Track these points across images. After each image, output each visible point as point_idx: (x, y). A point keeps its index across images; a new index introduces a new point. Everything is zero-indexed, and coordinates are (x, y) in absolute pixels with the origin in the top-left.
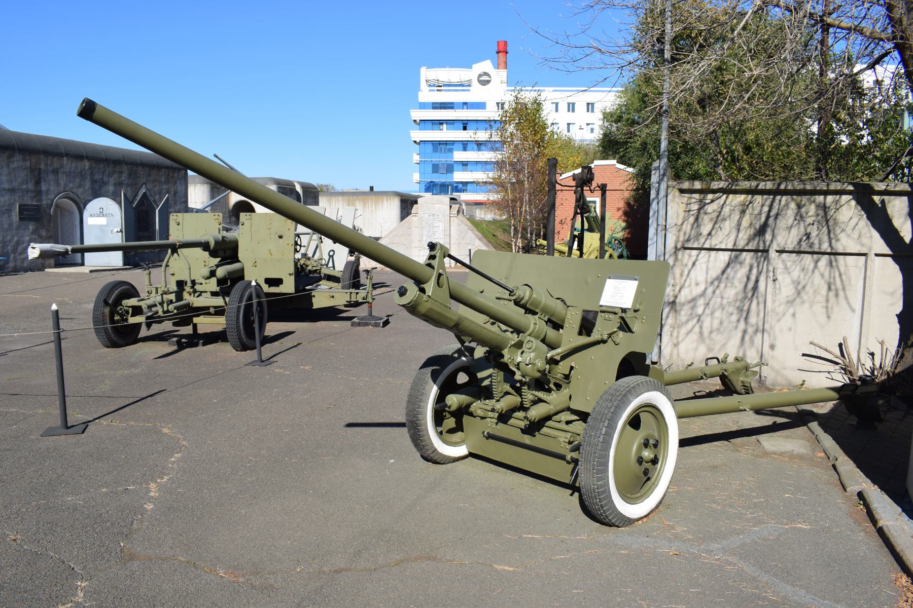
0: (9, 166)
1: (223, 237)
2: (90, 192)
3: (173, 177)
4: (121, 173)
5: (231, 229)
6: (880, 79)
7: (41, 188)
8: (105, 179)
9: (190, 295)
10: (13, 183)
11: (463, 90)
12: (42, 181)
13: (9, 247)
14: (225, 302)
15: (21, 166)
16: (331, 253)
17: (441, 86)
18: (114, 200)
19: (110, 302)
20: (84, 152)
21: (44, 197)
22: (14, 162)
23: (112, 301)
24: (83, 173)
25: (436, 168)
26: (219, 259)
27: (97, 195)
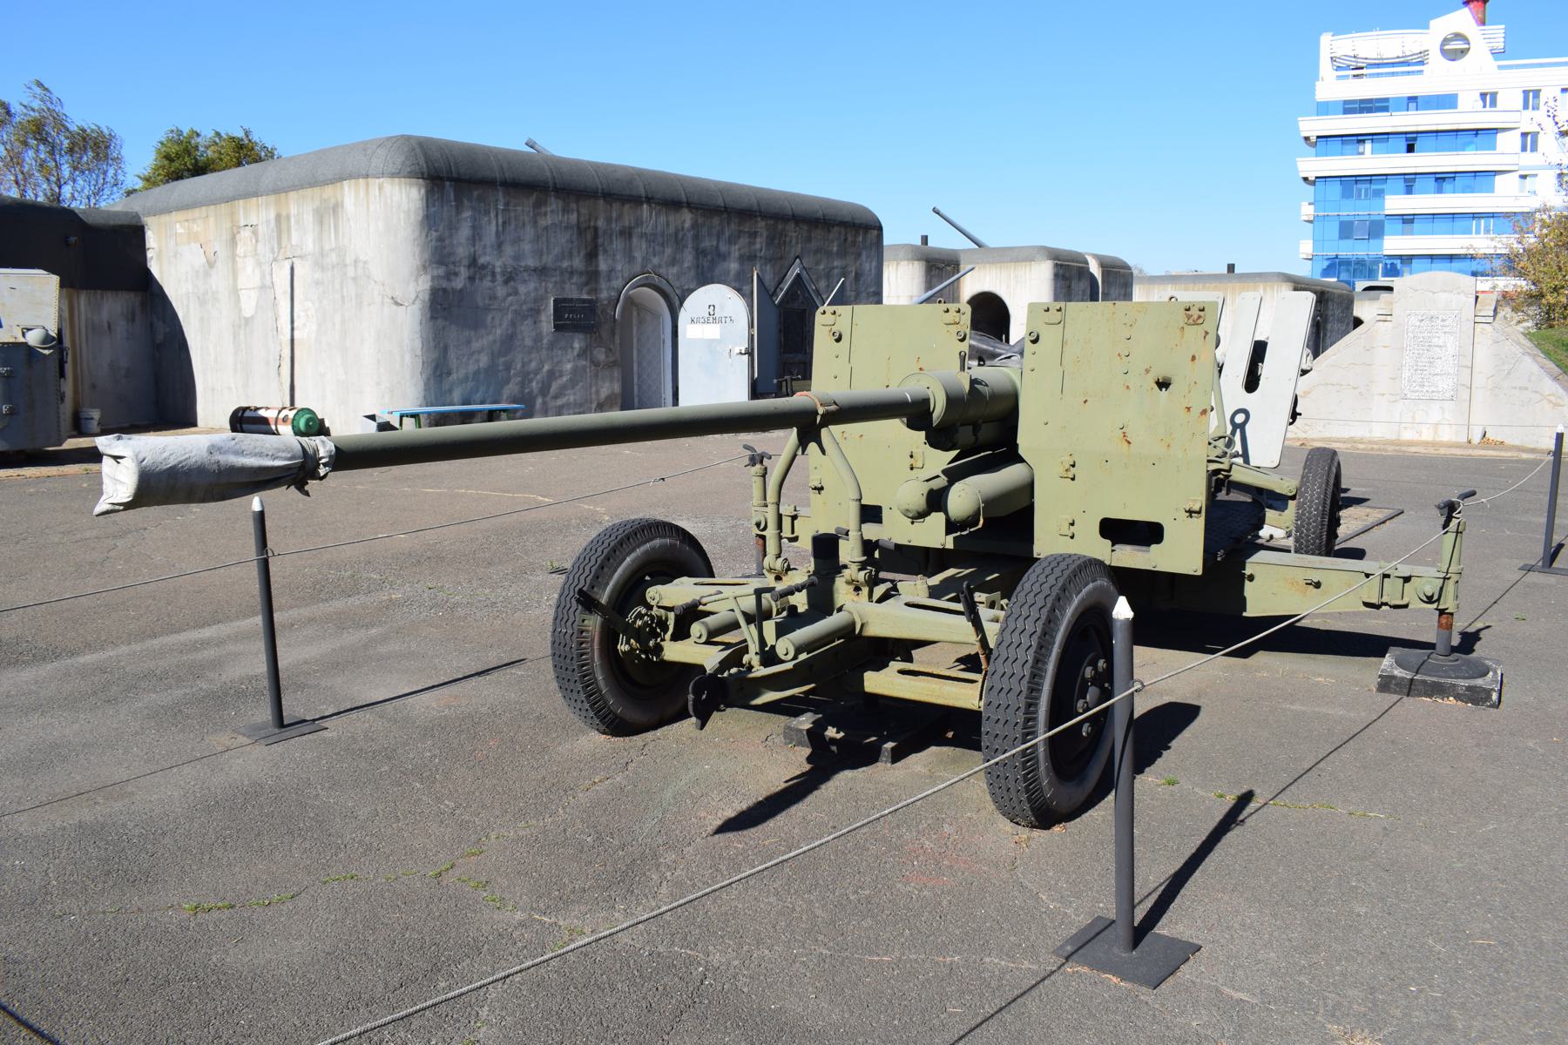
0: (536, 222)
1: (973, 382)
2: (693, 273)
3: (854, 243)
4: (754, 235)
5: (994, 356)
6: (312, 485)
7: (597, 266)
8: (723, 248)
9: (857, 589)
10: (544, 257)
11: (1409, 73)
12: (601, 253)
13: (534, 384)
14: (984, 642)
15: (561, 222)
16: (1240, 418)
17: (1362, 68)
18: (739, 290)
19: (604, 600)
20: (683, 196)
21: (603, 285)
22: (545, 214)
23: (610, 597)
24: (680, 236)
25: (1346, 230)
26: (954, 453)
27: (704, 279)
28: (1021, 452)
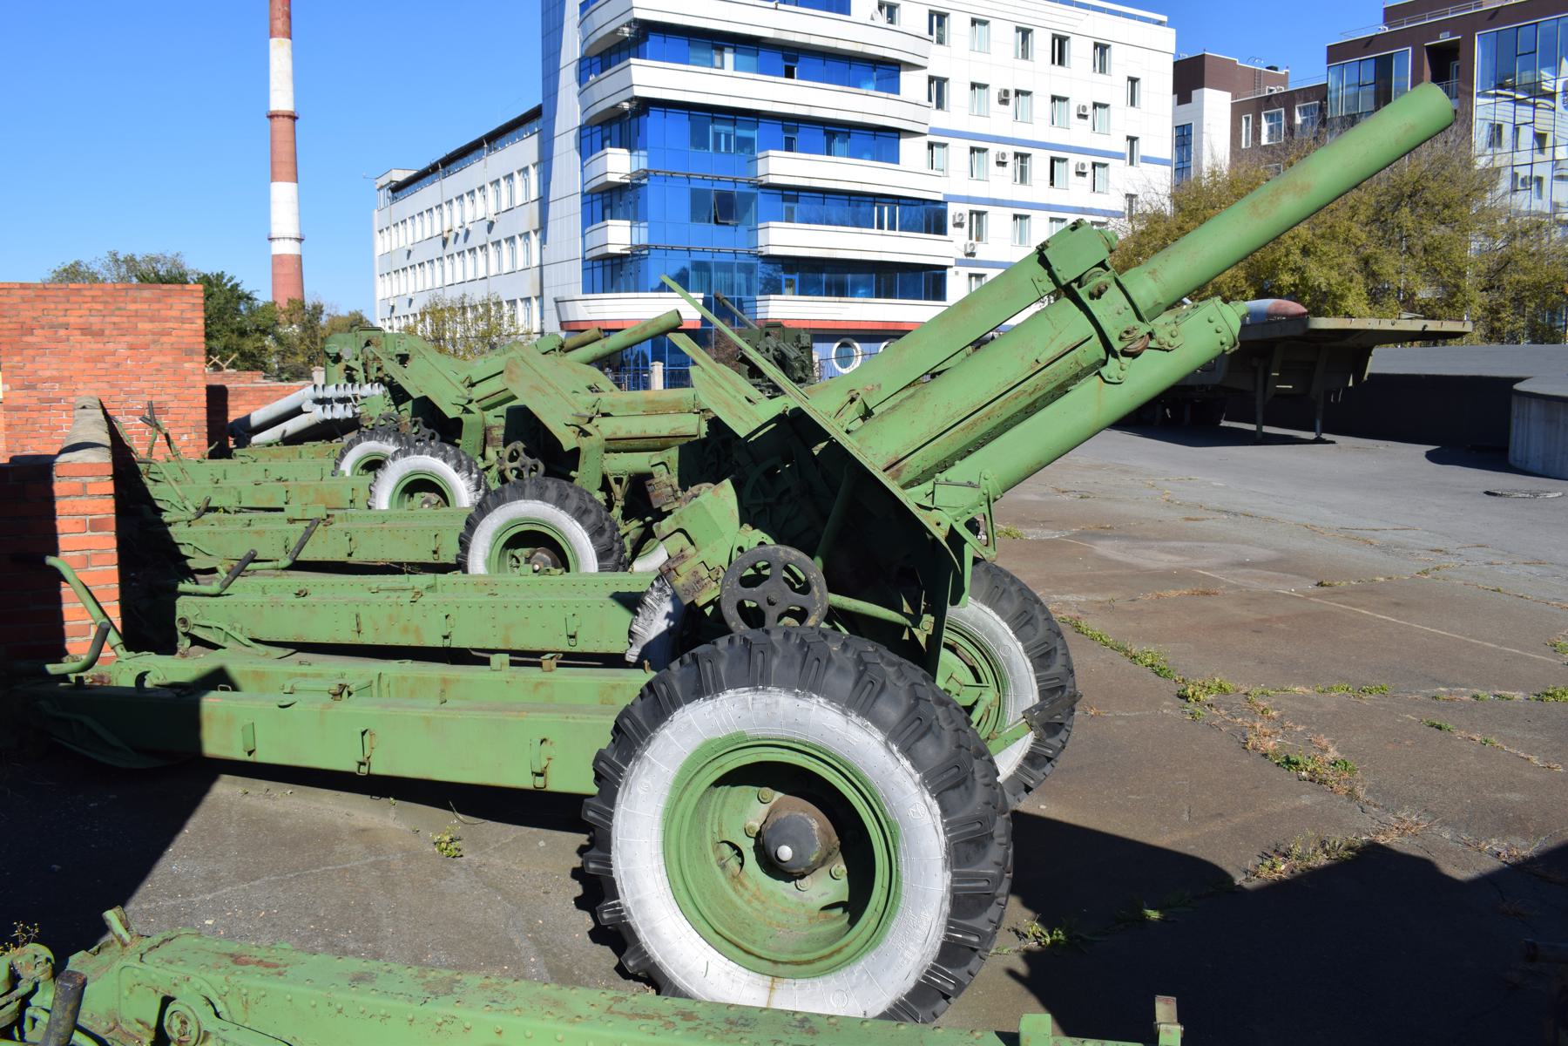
28: (196, 647)
